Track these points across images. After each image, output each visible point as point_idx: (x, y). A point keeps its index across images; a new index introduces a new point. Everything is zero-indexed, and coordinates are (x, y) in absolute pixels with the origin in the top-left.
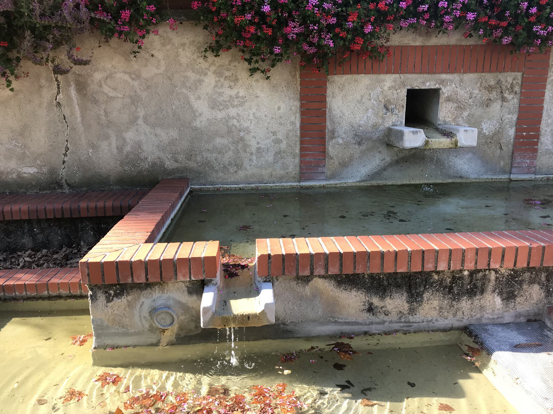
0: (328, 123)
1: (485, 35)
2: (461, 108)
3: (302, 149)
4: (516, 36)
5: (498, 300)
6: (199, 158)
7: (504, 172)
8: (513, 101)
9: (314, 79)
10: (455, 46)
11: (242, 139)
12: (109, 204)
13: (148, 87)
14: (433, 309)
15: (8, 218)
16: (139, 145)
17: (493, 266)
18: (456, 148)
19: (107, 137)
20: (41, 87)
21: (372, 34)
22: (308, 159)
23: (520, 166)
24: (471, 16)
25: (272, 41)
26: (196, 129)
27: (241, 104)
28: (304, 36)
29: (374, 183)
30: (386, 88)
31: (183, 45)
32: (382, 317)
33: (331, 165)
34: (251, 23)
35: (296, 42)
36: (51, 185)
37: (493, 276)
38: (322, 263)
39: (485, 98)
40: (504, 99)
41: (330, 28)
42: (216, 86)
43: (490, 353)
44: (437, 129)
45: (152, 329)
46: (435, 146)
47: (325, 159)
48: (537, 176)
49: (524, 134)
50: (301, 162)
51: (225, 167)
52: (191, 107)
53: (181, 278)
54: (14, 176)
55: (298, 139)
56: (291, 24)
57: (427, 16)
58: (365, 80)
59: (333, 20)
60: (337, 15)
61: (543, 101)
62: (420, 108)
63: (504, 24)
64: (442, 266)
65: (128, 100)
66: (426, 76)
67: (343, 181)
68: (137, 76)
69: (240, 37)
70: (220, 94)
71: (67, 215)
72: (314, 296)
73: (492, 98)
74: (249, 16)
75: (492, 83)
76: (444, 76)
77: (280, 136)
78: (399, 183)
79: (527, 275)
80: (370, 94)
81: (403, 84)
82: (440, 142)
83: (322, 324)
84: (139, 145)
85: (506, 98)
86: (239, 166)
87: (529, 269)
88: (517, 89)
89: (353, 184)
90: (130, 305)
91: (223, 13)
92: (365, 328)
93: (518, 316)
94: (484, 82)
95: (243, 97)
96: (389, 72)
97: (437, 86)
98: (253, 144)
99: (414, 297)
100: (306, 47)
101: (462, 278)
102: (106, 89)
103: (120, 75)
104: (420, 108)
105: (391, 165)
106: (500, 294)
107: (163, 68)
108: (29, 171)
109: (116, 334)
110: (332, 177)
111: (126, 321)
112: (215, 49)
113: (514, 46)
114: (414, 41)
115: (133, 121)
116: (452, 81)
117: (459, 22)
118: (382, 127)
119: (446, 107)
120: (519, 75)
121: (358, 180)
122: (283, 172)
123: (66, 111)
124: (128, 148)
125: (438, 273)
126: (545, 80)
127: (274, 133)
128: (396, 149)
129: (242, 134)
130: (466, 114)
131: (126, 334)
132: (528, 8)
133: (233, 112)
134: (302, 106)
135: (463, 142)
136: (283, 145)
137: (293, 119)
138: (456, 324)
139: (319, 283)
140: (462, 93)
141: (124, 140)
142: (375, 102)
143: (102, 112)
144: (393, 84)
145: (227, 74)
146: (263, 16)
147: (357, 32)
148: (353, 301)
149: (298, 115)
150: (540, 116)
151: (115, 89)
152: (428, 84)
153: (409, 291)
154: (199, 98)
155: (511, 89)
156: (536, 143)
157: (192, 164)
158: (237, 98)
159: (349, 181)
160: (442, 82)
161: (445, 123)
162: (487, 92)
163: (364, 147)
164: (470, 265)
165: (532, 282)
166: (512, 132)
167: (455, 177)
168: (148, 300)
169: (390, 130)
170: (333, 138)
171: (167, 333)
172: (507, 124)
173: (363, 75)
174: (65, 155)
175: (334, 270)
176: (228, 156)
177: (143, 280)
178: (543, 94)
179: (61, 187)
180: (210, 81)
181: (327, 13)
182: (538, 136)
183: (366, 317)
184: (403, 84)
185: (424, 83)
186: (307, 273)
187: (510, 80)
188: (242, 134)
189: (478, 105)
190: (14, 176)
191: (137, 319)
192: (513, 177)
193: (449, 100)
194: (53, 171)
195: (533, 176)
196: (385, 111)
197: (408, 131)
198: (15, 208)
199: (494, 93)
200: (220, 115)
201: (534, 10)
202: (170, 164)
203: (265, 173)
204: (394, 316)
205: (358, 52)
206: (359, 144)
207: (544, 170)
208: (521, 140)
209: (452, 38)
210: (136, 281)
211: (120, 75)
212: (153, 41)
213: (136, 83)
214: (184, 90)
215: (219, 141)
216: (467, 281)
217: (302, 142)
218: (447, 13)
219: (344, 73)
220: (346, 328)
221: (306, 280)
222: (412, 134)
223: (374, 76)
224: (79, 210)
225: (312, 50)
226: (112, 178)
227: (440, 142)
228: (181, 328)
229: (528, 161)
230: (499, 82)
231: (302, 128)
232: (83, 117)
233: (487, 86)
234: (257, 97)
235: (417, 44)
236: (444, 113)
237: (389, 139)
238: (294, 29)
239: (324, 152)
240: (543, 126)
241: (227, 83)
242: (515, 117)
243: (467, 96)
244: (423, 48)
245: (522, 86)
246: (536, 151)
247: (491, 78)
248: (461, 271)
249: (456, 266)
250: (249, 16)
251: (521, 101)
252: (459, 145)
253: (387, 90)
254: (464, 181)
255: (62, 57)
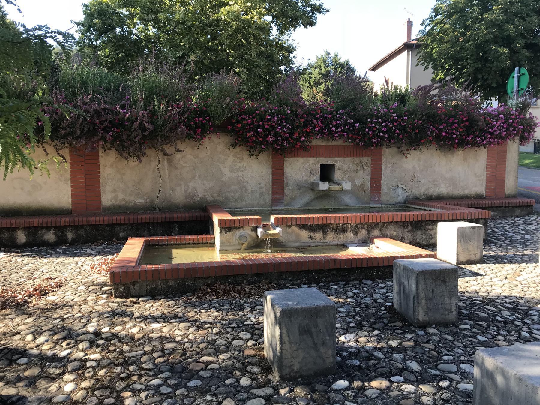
1: (352, 142)
2: (345, 173)
3: (272, 191)
4: (365, 142)
5: (352, 235)
7: (367, 203)
8: (368, 170)
10: (340, 145)
11: (244, 186)
12: (187, 215)
13: (202, 162)
14: (330, 237)
15: (139, 221)
16: (195, 189)
17: (349, 222)
18: (342, 191)
19: (180, 185)
20: (151, 161)
21: (304, 141)
22: (276, 196)
24: (345, 134)
25: (261, 143)
26: (223, 181)
27: (245, 170)
28: (276, 141)
29: (307, 208)
31: (219, 143)
32: (314, 240)
33: (286, 199)
34: (253, 135)
35: (272, 144)
36: (150, 208)
37: (350, 226)
38: (295, 220)
40: (364, 169)
41: (286, 138)
42: (233, 162)
43: (348, 248)
44: (334, 183)
45: (239, 244)
46: (333, 189)
50: (272, 197)
51: (236, 200)
52: (221, 171)
53: (250, 225)
54: (133, 204)
55: (271, 187)
56: (270, 136)
57: (327, 134)
58: (301, 160)
59: (288, 135)
60: (289, 133)
62: (326, 173)
63: (360, 137)
64: (333, 222)
65: (192, 168)
66: (328, 158)
68: (196, 156)
69: (248, 142)
70: (235, 165)
71: (167, 220)
72: (292, 232)
74: (252, 133)
75: (358, 162)
76: (336, 158)
77: (262, 185)
78: (318, 208)
79: (361, 226)
81: (318, 162)
82: (335, 188)
83: (295, 243)
84: (195, 189)
86: (242, 199)
87: (361, 224)
88: (369, 164)
90: (232, 235)
91: (241, 132)
92: (309, 244)
93: (359, 241)
95: (245, 167)
96: (312, 156)
97: (333, 163)
98: (250, 189)
99: (325, 234)
100: (276, 146)
101: (339, 227)
102: (181, 162)
103: (188, 156)
104: (326, 173)
105: (314, 199)
106: (353, 232)
107: (209, 153)
108: (140, 201)
109: (227, 246)
110: (287, 205)
111: (231, 241)
112: (234, 145)
113: (366, 146)
115: (193, 178)
116: (340, 161)
117: (341, 136)
118: (309, 182)
120: (370, 158)
122: (263, 202)
123: (162, 172)
124: (190, 191)
125: (332, 224)
127: (260, 184)
128: (316, 192)
129: (244, 184)
130: (347, 176)
131: (230, 246)
132: (369, 131)
133: (240, 174)
136: (264, 190)
137: (268, 177)
138: (339, 243)
139: (294, 228)
140: (345, 166)
141: (188, 187)
143: (179, 173)
145: (239, 156)
146: (258, 133)
147: (298, 140)
148: (305, 234)
149: (271, 176)
151: (186, 162)
153: (323, 231)
154: (225, 167)
155: (367, 165)
157: (220, 199)
160: (336, 161)
161: (338, 179)
163: (301, 191)
164: (342, 222)
165: (362, 228)
167: (344, 206)
168: (238, 233)
169: (313, 183)
170: (287, 186)
171: (244, 245)
174: (159, 193)
175: (299, 223)
176: (237, 195)
177: (238, 226)
179: (155, 209)
180: (231, 159)
181: (286, 132)
182: (381, 186)
183: (309, 240)
184: (318, 162)
186: (290, 224)
187: (366, 161)
188: (244, 184)
190: (133, 204)
191: (234, 240)
192: (371, 205)
194: (152, 202)
195: (381, 205)
197: (321, 183)
198: (143, 217)
200: (234, 175)
201: (371, 132)
202: (209, 199)
203: (255, 203)
204: (318, 240)
205: (299, 148)
206: (299, 189)
209: (339, 142)
210: (236, 226)
211: (188, 156)
212: (206, 141)
213: (196, 160)
214: (218, 164)
215: (233, 187)
216: (341, 227)
217: (273, 188)
218: (335, 133)
220: (303, 244)
221: (289, 227)
223: (305, 158)
224: (173, 218)
225: (279, 147)
226: (181, 205)
227: (335, 188)
228: (248, 244)
230: (361, 161)
231: (273, 181)
232: (169, 175)
235: (324, 144)
236: (337, 175)
237: (313, 187)
238: (271, 138)
239: (283, 193)
240: (382, 181)
241: (238, 161)
242: (369, 177)
243: (347, 167)
246: (380, 193)
247: (357, 160)
248: (339, 224)
249: (337, 222)
250: (252, 133)
251: (372, 170)
254: (348, 207)
255: (169, 149)
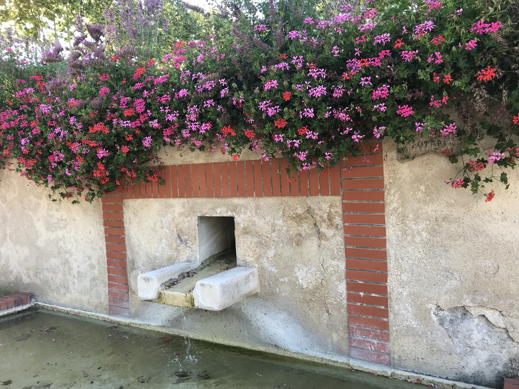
0: (128, 252)
6: (41, 276)
8: (336, 240)
9: (112, 203)
23: (361, 346)
27: (65, 227)
30: (176, 215)
39: (293, 232)
40: (320, 236)
42: (48, 209)
47: (128, 293)
48: (399, 372)
49: (362, 294)
61: (383, 243)
66: (215, 200)
67: (146, 322)
73: (303, 233)
76: (236, 201)
80: (162, 221)
85: (324, 234)
88: (338, 220)
89: (157, 329)
94: (287, 209)
110: (136, 315)
114: (197, 158)
116: (246, 208)
119: (244, 242)
121: (160, 324)
126: (382, 208)
127: (89, 258)
130: (271, 253)
134: (106, 231)
135: (201, 301)
140: (262, 224)
142: (167, 231)
144: (182, 210)
150: (384, 267)
152: (219, 210)
154: (39, 220)
156: (385, 313)
157: (38, 282)
158: (62, 220)
159: (153, 324)
160: (235, 208)
162: (295, 224)
166: (342, 288)
170: (133, 269)
172: (332, 274)
173: (152, 199)
176: (59, 278)
178: (383, 231)
185: (214, 209)
187: (325, 206)
189: (285, 242)
193: (247, 233)
196: (179, 241)
199: (305, 226)
202: (26, 280)
207: (411, 364)
208: (359, 304)
219: (137, 197)
222: (144, 281)
223: (163, 201)
229: (375, 341)
230: (309, 210)
233: (294, 216)
234: (75, 220)
240: (392, 283)
244: (207, 166)
245: (345, 219)
246: (385, 326)
247: (297, 204)
252: (196, 304)
253: (178, 217)
254: (280, 353)
